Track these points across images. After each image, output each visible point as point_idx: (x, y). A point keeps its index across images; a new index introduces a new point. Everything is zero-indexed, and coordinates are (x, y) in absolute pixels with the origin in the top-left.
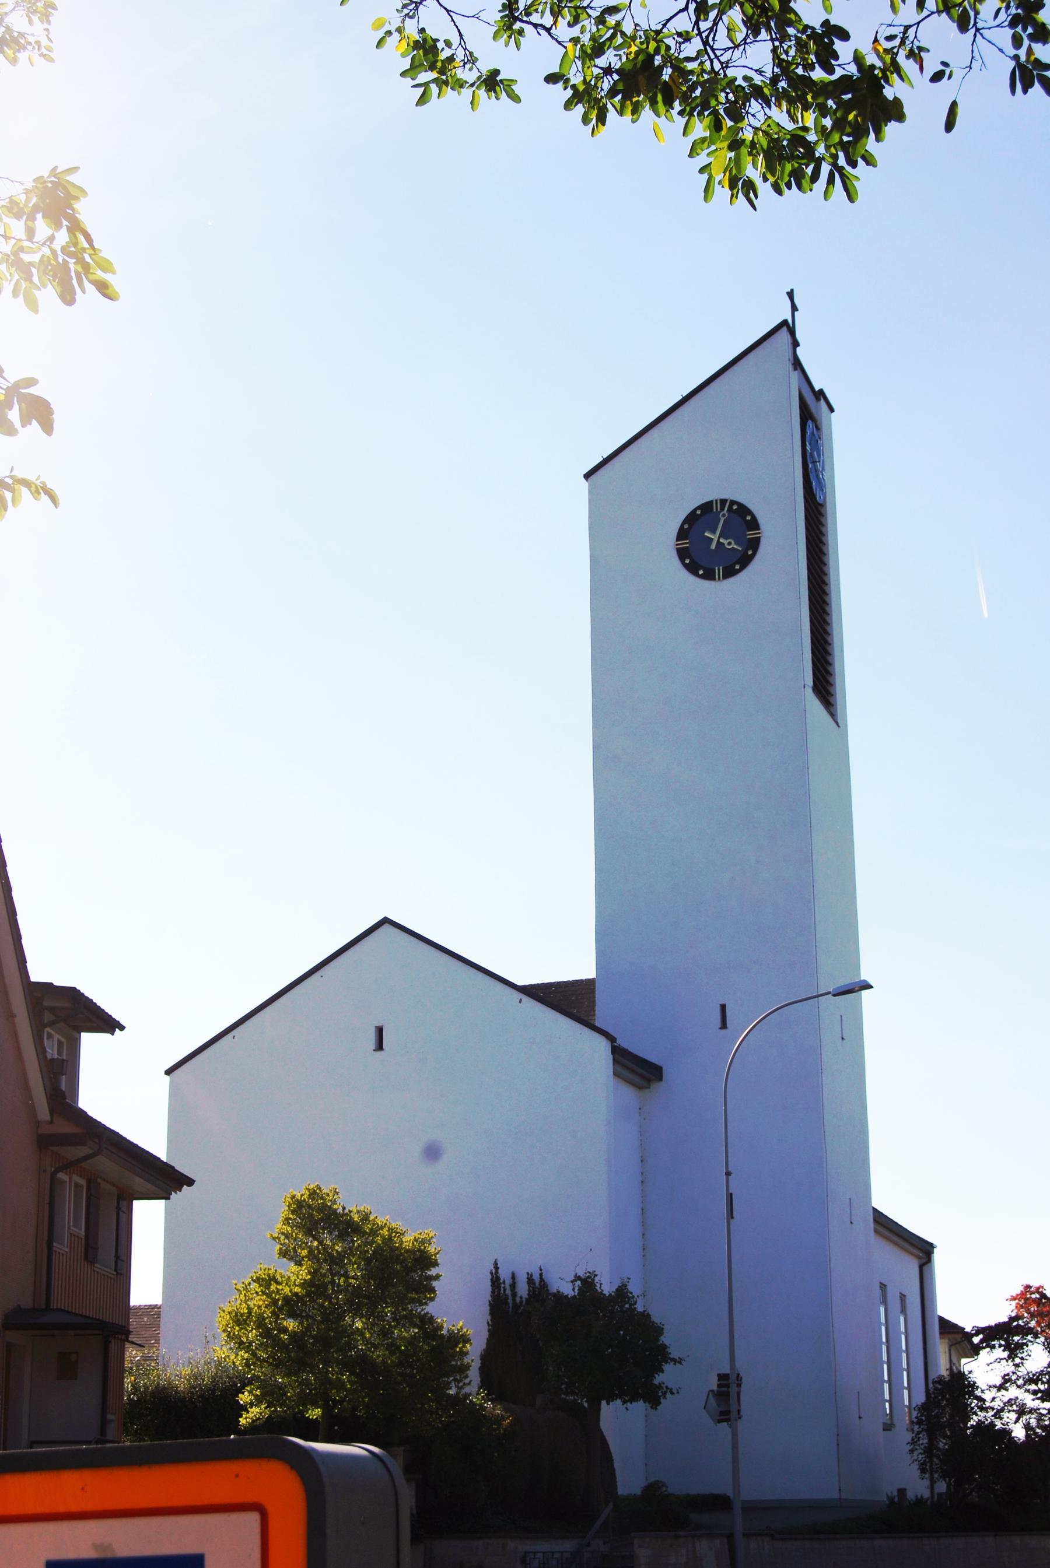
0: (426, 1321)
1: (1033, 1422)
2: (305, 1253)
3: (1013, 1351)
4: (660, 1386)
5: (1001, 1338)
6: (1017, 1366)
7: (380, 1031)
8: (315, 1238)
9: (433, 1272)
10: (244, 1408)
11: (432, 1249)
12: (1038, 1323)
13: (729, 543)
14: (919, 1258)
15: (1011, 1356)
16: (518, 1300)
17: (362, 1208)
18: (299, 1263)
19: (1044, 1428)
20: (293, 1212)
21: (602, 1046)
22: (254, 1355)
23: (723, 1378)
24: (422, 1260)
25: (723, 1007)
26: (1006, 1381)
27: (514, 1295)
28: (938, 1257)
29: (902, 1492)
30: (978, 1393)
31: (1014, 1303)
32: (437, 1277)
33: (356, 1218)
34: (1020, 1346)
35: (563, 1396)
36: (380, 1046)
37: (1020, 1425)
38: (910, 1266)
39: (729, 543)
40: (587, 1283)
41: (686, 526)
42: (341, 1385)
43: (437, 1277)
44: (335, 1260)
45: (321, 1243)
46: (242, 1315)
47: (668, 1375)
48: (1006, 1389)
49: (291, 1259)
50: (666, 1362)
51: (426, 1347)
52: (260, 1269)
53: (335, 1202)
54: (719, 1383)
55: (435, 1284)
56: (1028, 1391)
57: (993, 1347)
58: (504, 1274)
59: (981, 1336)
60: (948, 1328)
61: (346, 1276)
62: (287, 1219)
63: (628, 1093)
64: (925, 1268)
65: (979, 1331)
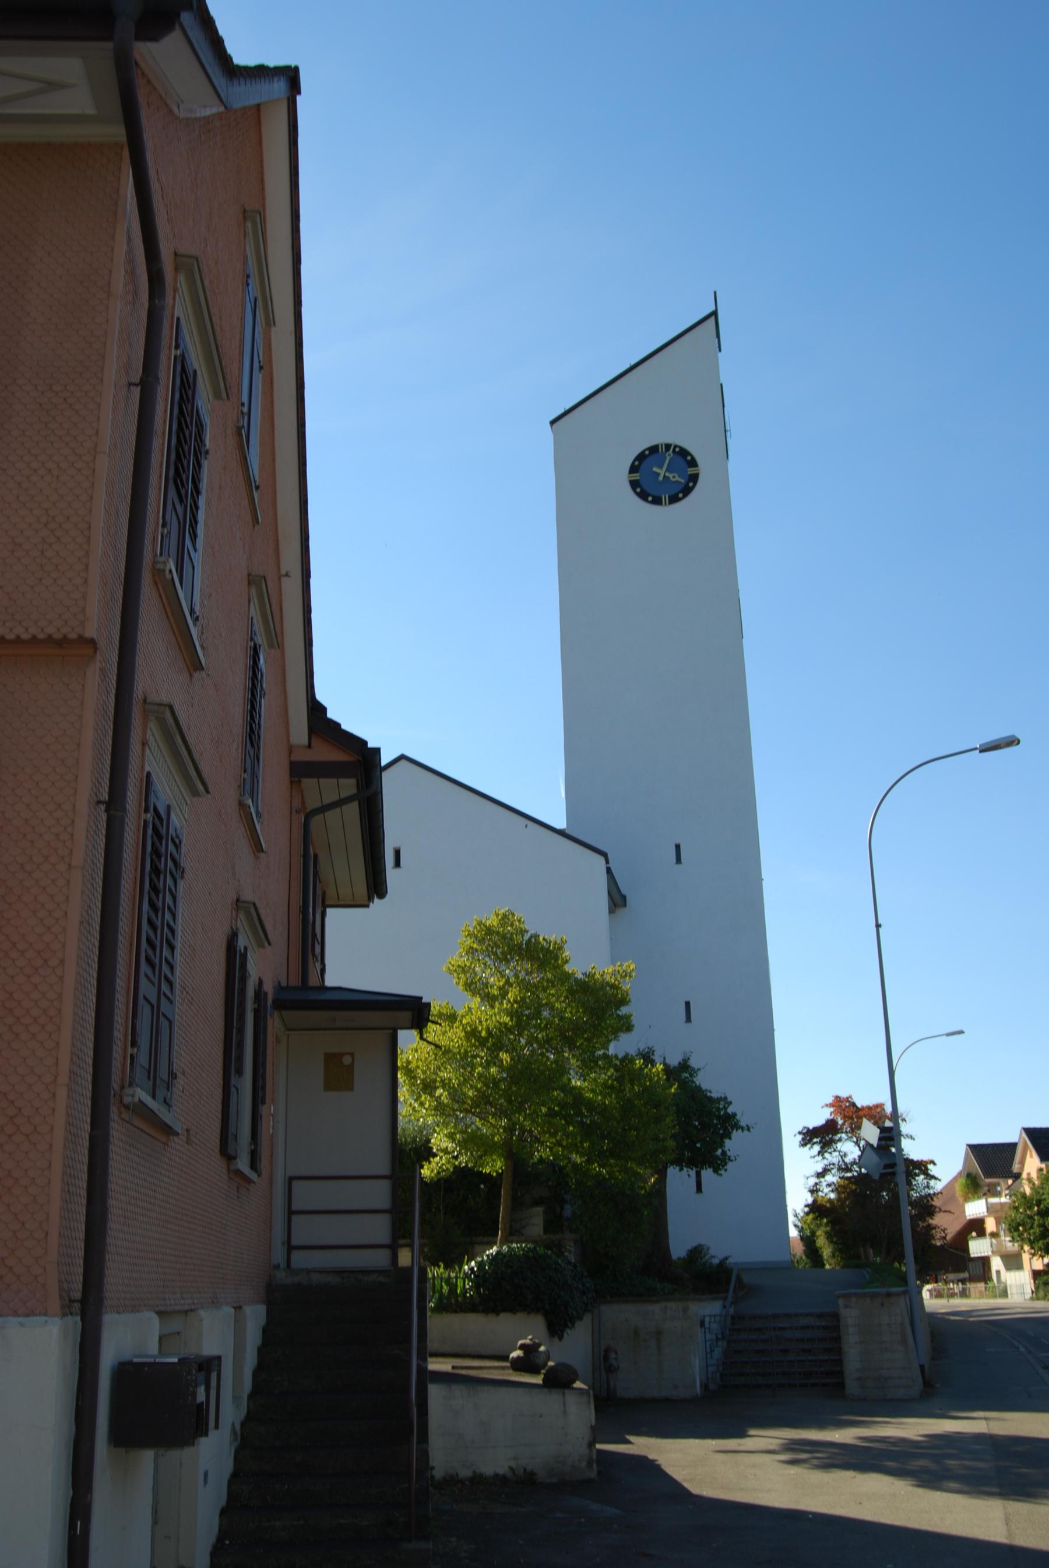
13: (674, 477)
39: (674, 477)
54: (882, 1135)
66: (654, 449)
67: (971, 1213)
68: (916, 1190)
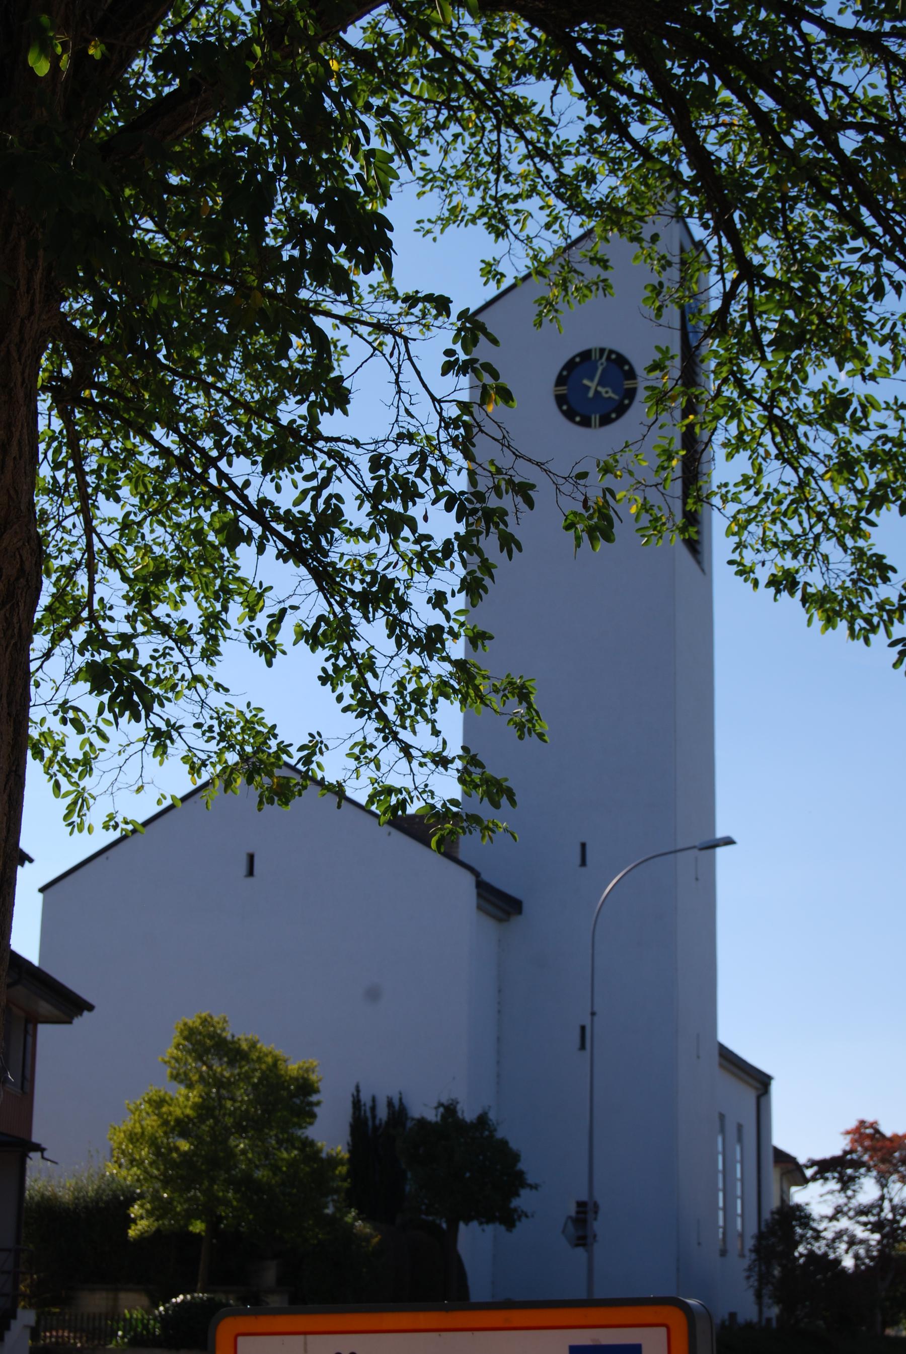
0: (307, 1145)
1: (862, 1252)
2: (195, 1078)
3: (846, 1183)
4: (515, 1210)
5: (834, 1170)
6: (849, 1198)
7: (251, 858)
8: (204, 1063)
9: (314, 1098)
10: (134, 1221)
11: (313, 1077)
12: (871, 1157)
13: (607, 393)
14: (756, 1089)
15: (844, 1189)
16: (377, 1122)
17: (250, 1037)
18: (190, 1086)
19: (872, 1258)
20: (186, 1038)
21: (468, 880)
22: (146, 1171)
23: (581, 1205)
24: (306, 1087)
25: (583, 846)
26: (839, 1212)
27: (374, 1117)
28: (776, 1088)
29: (733, 1316)
30: (814, 1225)
31: (849, 1137)
32: (318, 1103)
33: (244, 1046)
34: (852, 1179)
35: (423, 1217)
36: (251, 872)
37: (851, 1254)
38: (749, 1095)
39: (607, 393)
40: (449, 1110)
41: (565, 373)
42: (227, 1203)
43: (318, 1103)
44: (220, 1083)
45: (210, 1067)
46: (136, 1134)
47: (523, 1201)
48: (838, 1220)
49: (181, 1082)
50: (523, 1187)
51: (307, 1169)
52: (153, 1091)
53: (223, 1029)
55: (316, 1110)
56: (858, 1222)
57: (826, 1179)
58: (365, 1098)
59: (815, 1169)
60: (783, 1159)
61: (233, 1099)
62: (178, 1045)
63: (489, 923)
64: (763, 1100)
65: (813, 1163)
66: (586, 355)
67: (39, 1185)
68: (140, 1122)
